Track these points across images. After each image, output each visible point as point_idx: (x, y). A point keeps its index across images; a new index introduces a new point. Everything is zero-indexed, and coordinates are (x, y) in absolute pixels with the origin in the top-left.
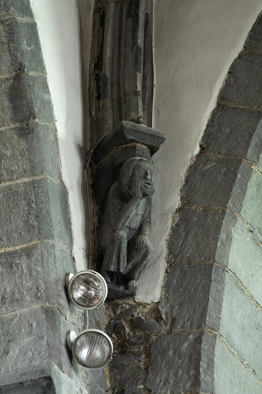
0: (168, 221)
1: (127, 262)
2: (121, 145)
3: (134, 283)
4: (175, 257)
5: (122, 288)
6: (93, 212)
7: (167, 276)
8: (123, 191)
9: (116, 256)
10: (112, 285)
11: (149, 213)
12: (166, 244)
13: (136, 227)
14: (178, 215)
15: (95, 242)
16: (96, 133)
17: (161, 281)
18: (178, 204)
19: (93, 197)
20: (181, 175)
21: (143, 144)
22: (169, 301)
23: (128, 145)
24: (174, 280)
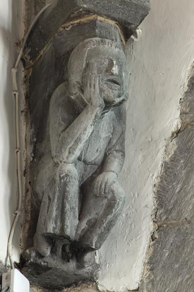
0: (158, 152)
1: (79, 219)
2: (72, 20)
3: (98, 256)
4: (168, 212)
5: (72, 265)
6: (26, 140)
7: (154, 245)
8: (73, 97)
9: (58, 207)
10: (54, 260)
11: (121, 135)
12: (154, 192)
13: (97, 160)
14: (174, 141)
15: (28, 189)
16: (34, 9)
17: (143, 254)
18: (176, 124)
19: (26, 115)
20: (183, 75)
21: (108, 17)
22: (156, 286)
23: (82, 20)
24: (164, 250)
